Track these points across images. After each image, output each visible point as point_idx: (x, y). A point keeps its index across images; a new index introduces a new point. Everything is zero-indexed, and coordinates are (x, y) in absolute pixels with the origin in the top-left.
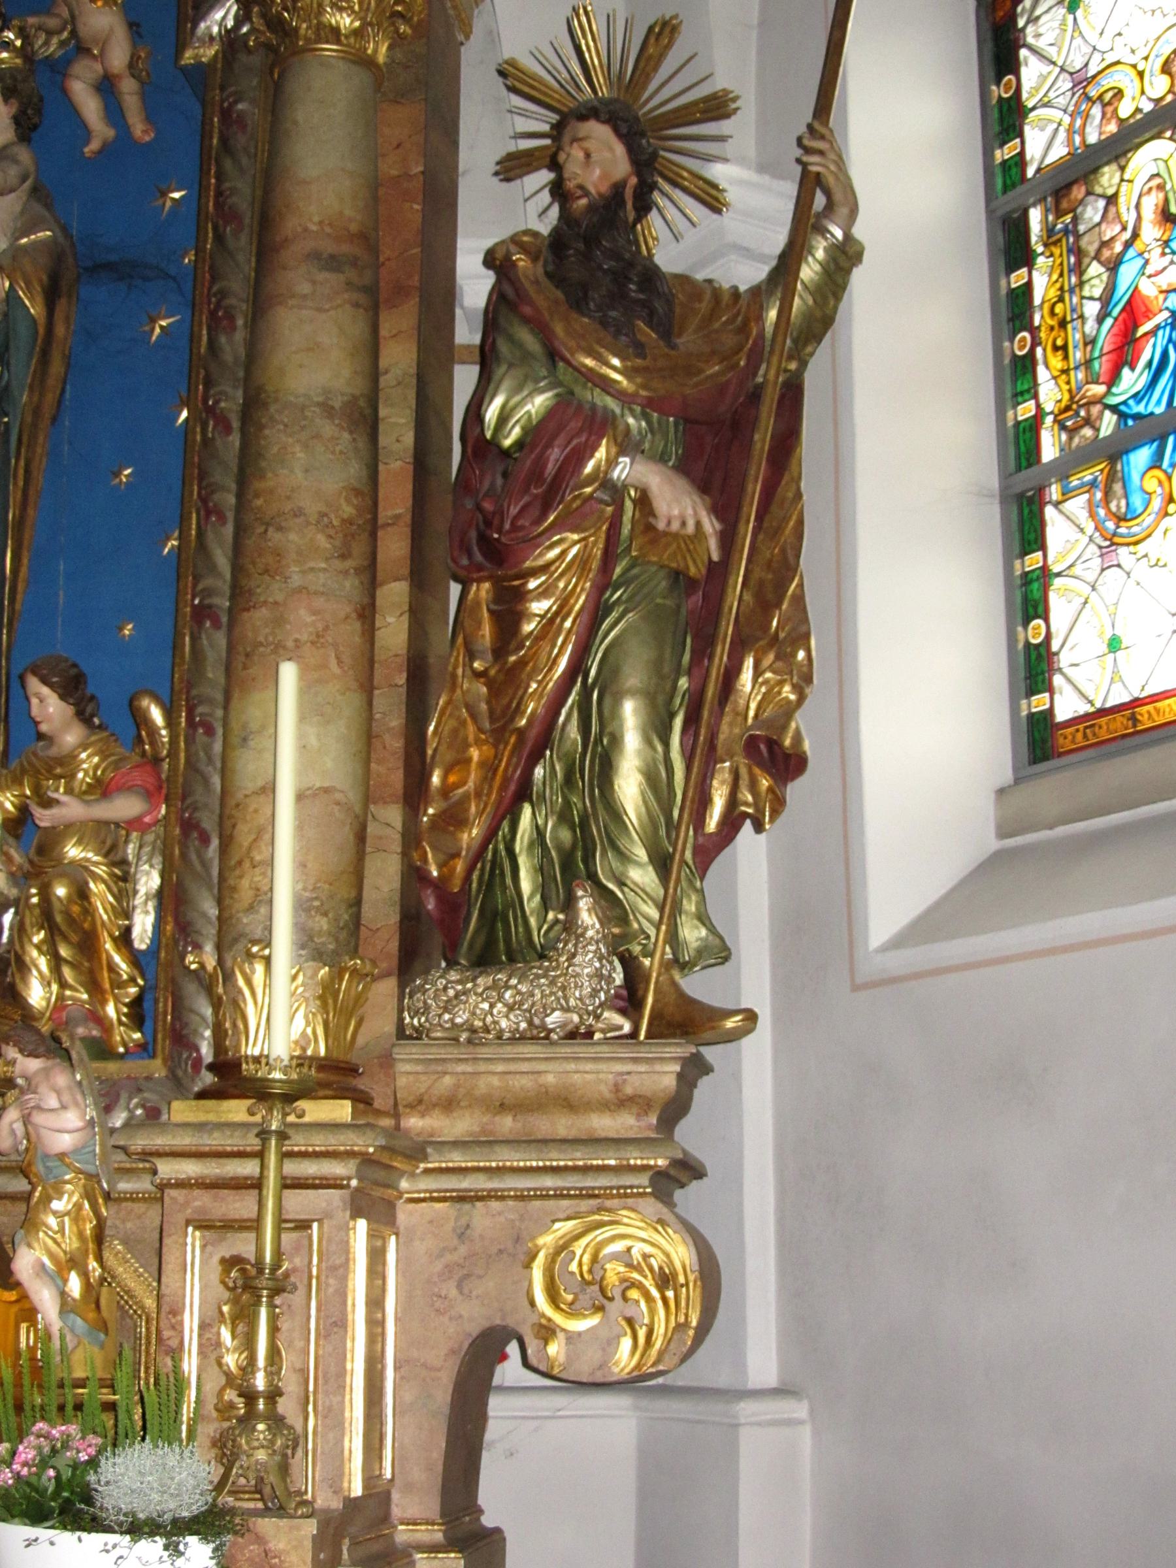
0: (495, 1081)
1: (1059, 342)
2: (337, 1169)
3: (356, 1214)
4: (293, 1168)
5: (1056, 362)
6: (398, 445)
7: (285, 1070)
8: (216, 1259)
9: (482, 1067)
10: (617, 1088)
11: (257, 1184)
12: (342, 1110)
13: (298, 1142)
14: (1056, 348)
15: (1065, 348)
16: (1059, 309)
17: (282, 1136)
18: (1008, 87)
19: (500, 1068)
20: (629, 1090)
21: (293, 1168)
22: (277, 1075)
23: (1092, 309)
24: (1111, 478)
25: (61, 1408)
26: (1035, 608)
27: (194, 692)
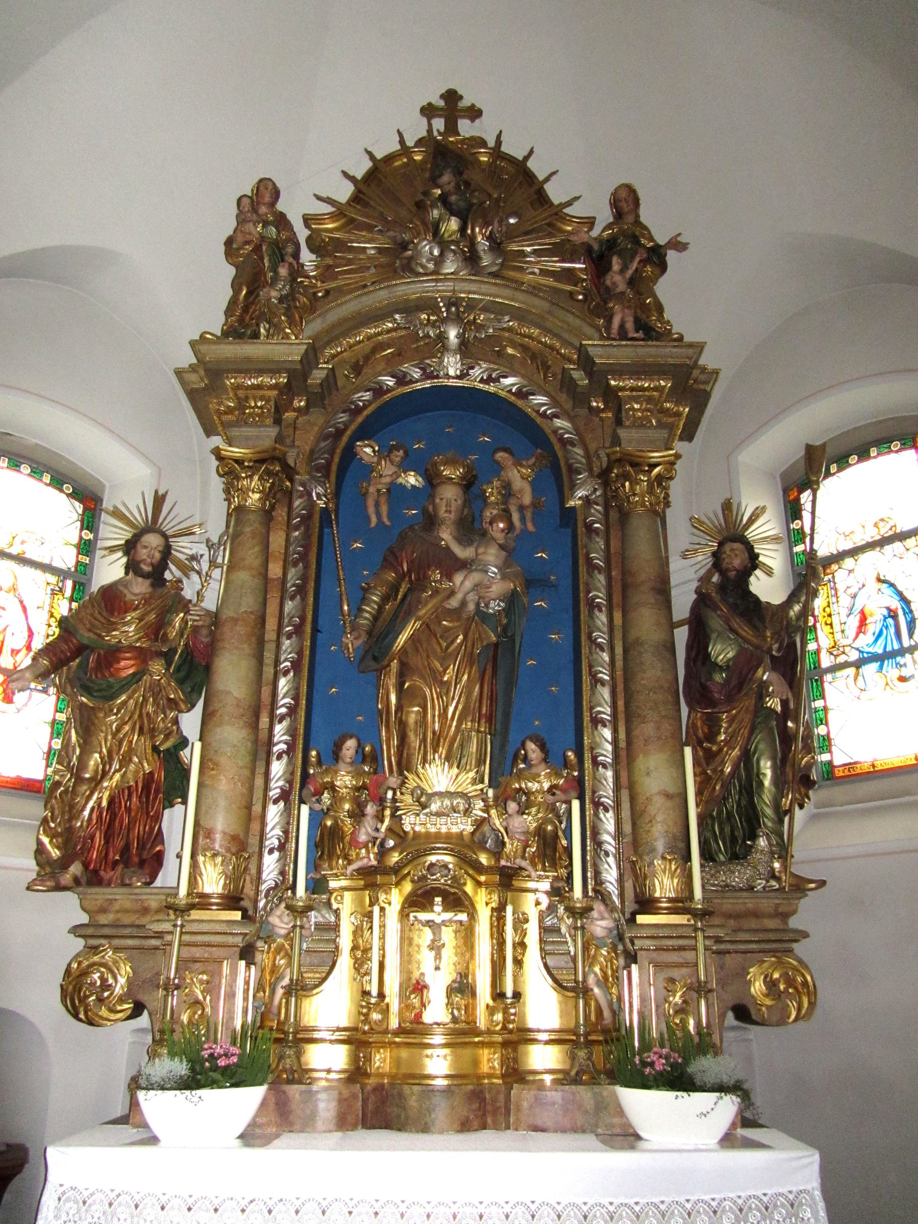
0: (730, 906)
1: (828, 622)
2: (230, 940)
3: (241, 959)
4: (186, 938)
5: (827, 629)
6: (51, 623)
7: (581, 902)
8: (661, 979)
9: (725, 901)
10: (776, 910)
11: (695, 949)
12: (237, 915)
13: (187, 928)
14: (826, 624)
15: (831, 625)
16: (827, 610)
17: (182, 926)
18: (797, 524)
19: (731, 901)
20: (780, 910)
21: (186, 938)
22: (578, 905)
23: (843, 612)
24: (857, 675)
25: (612, 1040)
26: (821, 721)
27: (595, 752)
